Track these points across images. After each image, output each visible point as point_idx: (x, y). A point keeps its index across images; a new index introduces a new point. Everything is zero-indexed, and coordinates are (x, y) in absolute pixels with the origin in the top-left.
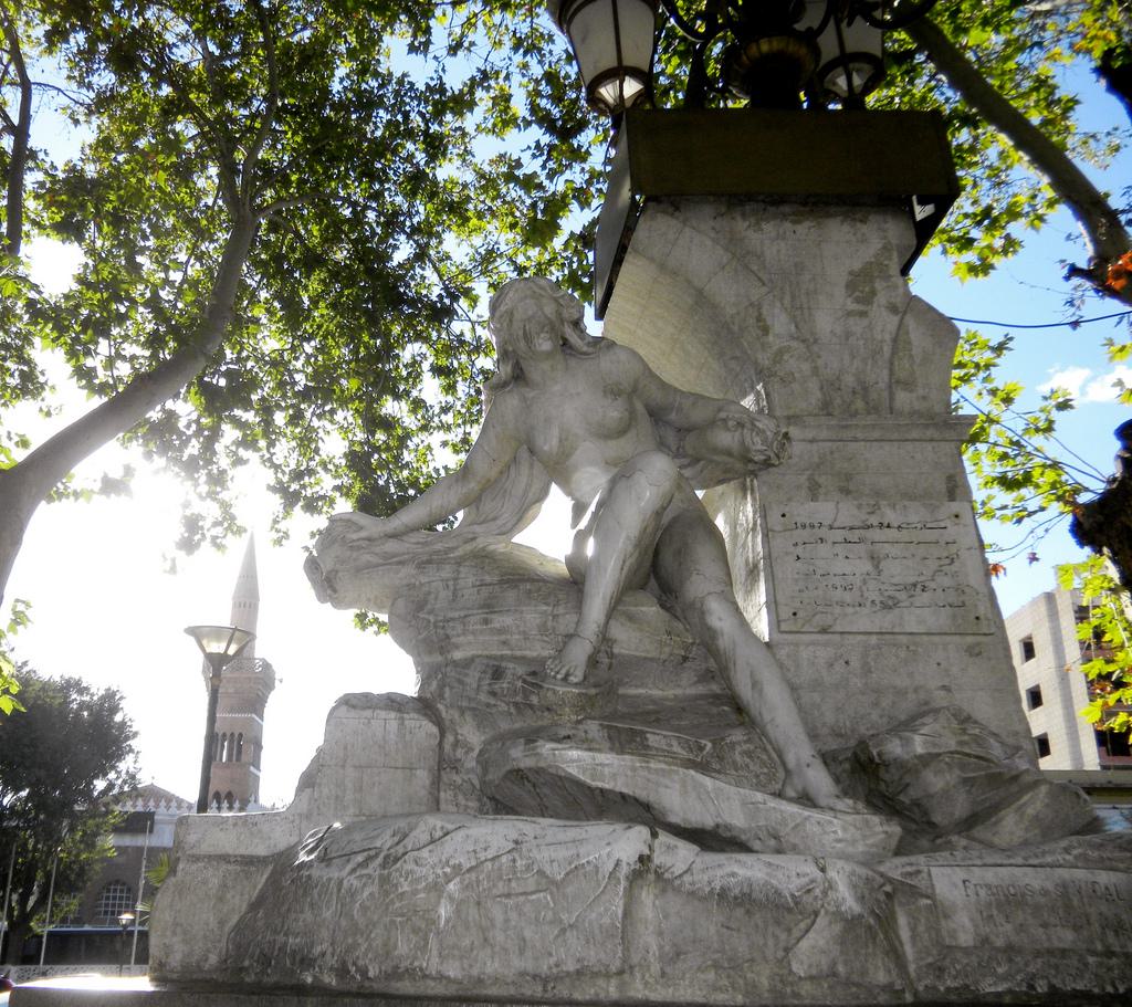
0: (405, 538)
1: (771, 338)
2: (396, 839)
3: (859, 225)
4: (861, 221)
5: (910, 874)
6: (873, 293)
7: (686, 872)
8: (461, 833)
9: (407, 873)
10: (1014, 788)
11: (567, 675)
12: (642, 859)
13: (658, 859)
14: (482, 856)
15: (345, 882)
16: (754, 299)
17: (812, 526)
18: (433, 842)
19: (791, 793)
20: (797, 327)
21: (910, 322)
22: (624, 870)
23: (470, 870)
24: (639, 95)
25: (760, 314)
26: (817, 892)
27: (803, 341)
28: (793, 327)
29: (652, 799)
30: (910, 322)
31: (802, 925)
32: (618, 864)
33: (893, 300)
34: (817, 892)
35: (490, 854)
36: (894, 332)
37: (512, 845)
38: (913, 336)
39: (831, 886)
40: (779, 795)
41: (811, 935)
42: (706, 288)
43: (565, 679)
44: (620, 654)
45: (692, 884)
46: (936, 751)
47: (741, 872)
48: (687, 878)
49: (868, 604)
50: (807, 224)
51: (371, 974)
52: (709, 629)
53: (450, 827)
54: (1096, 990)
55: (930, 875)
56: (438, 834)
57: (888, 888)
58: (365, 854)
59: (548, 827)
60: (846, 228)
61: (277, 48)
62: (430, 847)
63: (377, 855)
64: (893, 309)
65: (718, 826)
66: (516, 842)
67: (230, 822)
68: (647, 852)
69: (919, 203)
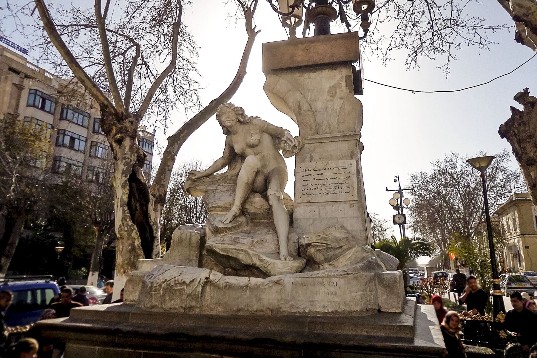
1: (302, 111)
13: (211, 278)
14: (171, 277)
25: (300, 104)
33: (342, 95)
48: (218, 282)
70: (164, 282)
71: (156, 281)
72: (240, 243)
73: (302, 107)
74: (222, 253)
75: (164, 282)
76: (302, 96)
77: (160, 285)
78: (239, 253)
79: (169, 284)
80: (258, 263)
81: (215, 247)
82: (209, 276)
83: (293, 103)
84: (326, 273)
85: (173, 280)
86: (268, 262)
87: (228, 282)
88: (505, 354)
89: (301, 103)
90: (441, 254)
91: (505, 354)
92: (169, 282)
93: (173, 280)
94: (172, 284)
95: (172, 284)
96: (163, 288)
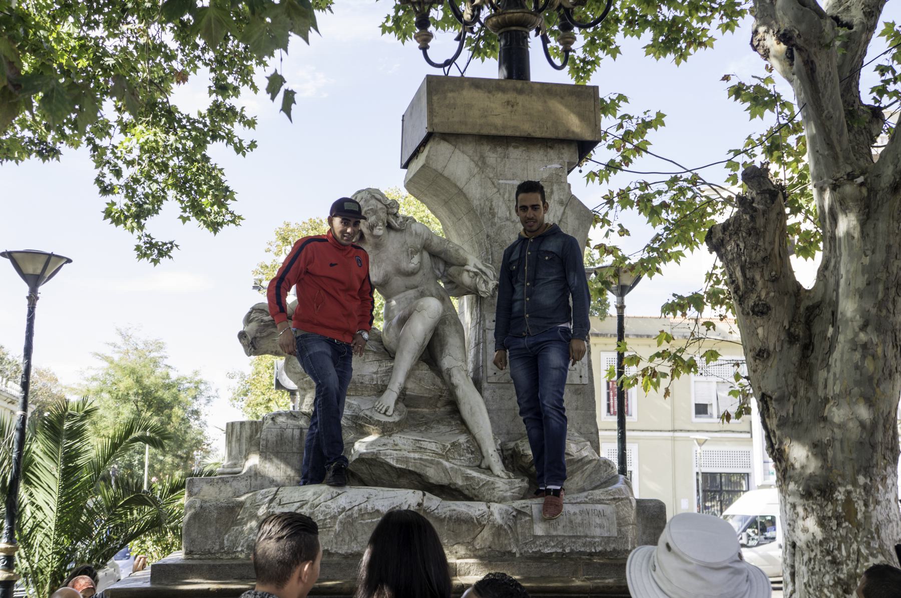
1: (496, 220)
2: (315, 497)
3: (549, 150)
4: (550, 147)
5: (524, 507)
8: (345, 494)
9: (322, 512)
10: (580, 463)
11: (386, 411)
13: (425, 504)
14: (354, 504)
16: (489, 195)
18: (332, 498)
19: (483, 466)
20: (510, 213)
21: (569, 212)
23: (350, 509)
25: (492, 205)
27: (513, 222)
28: (508, 213)
29: (422, 472)
30: (569, 212)
31: (479, 529)
33: (562, 197)
36: (560, 217)
38: (569, 220)
39: (492, 514)
41: (482, 533)
42: (464, 189)
43: (385, 413)
44: (410, 395)
45: (438, 513)
47: (457, 509)
48: (436, 511)
50: (521, 149)
52: (452, 384)
53: (340, 492)
56: (335, 495)
57: (514, 513)
60: (541, 152)
61: (231, 35)
63: (307, 503)
64: (561, 203)
65: (450, 484)
66: (368, 498)
67: (215, 481)
68: (421, 501)
70: (340, 513)
71: (324, 511)
72: (794, 555)
73: (496, 211)
74: (398, 466)
75: (340, 513)
76: (495, 190)
77: (334, 517)
78: (425, 466)
79: (350, 516)
80: (460, 482)
81: (385, 455)
82: (423, 500)
83: (479, 200)
84: (589, 497)
85: (356, 508)
86: (482, 480)
87: (454, 510)
88: (41, 94)
89: (494, 204)
90: (788, 49)
91: (41, 94)
92: (350, 512)
93: (356, 508)
94: (356, 515)
95: (356, 515)
96: (341, 522)
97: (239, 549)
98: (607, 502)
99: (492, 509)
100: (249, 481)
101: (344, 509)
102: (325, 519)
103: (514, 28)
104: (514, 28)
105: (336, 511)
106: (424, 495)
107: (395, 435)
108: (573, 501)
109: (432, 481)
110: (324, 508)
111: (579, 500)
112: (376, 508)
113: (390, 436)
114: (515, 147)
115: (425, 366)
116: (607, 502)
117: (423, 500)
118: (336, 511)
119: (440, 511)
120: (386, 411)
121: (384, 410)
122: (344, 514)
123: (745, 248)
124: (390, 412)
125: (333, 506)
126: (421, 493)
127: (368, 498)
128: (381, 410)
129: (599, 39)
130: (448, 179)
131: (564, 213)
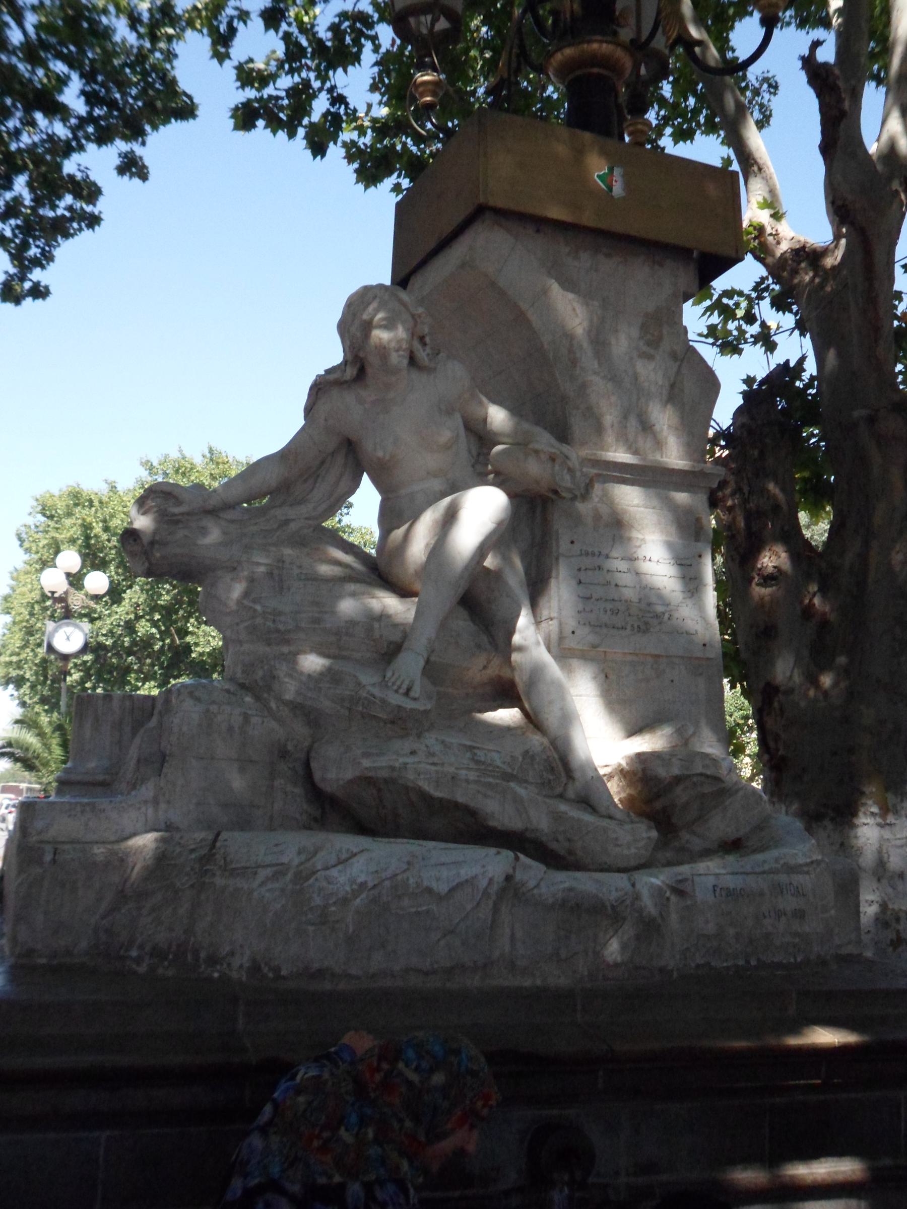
0: (221, 515)
2: (303, 857)
3: (656, 267)
6: (660, 338)
7: (535, 887)
12: (509, 878)
13: (519, 876)
15: (255, 894)
17: (593, 554)
19: (571, 794)
22: (495, 888)
23: (375, 886)
24: (445, 32)
26: (628, 902)
32: (491, 881)
34: (628, 902)
35: (389, 873)
37: (405, 867)
40: (561, 796)
46: (689, 773)
48: (535, 891)
49: (629, 627)
51: (284, 973)
54: (784, 961)
55: (693, 881)
58: (275, 869)
59: (435, 850)
62: (340, 867)
65: (527, 829)
66: (409, 863)
68: (511, 871)
69: (629, 113)
73: (578, 355)
74: (438, 794)
75: (355, 894)
77: (345, 901)
82: (514, 868)
85: (387, 883)
92: (375, 892)
97: (134, 953)
98: (805, 869)
99: (638, 886)
100: (143, 809)
101: (363, 885)
102: (326, 907)
103: (595, 70)
104: (595, 70)
105: (348, 888)
106: (517, 859)
107: (427, 735)
108: (757, 870)
109: (492, 823)
110: (324, 884)
111: (766, 867)
112: (426, 883)
113: (419, 736)
114: (608, 256)
115: (463, 613)
116: (805, 869)
117: (514, 868)
118: (348, 888)
119: (544, 890)
120: (409, 690)
121: (405, 687)
122: (364, 896)
123: (749, 493)
124: (416, 692)
125: (342, 879)
126: (510, 854)
127: (409, 863)
128: (399, 687)
129: (389, 325)
130: (502, 293)
131: (678, 372)
